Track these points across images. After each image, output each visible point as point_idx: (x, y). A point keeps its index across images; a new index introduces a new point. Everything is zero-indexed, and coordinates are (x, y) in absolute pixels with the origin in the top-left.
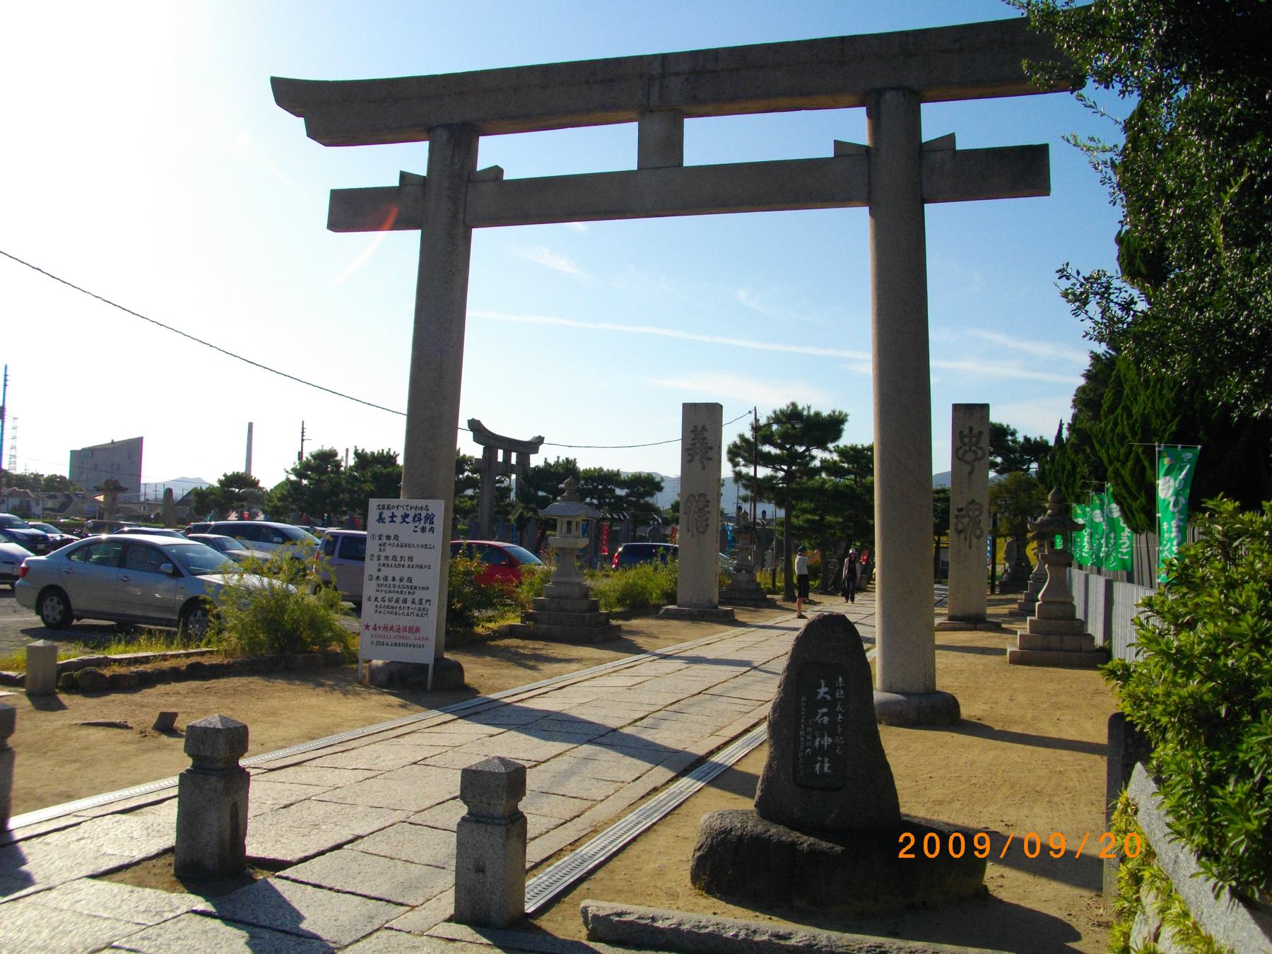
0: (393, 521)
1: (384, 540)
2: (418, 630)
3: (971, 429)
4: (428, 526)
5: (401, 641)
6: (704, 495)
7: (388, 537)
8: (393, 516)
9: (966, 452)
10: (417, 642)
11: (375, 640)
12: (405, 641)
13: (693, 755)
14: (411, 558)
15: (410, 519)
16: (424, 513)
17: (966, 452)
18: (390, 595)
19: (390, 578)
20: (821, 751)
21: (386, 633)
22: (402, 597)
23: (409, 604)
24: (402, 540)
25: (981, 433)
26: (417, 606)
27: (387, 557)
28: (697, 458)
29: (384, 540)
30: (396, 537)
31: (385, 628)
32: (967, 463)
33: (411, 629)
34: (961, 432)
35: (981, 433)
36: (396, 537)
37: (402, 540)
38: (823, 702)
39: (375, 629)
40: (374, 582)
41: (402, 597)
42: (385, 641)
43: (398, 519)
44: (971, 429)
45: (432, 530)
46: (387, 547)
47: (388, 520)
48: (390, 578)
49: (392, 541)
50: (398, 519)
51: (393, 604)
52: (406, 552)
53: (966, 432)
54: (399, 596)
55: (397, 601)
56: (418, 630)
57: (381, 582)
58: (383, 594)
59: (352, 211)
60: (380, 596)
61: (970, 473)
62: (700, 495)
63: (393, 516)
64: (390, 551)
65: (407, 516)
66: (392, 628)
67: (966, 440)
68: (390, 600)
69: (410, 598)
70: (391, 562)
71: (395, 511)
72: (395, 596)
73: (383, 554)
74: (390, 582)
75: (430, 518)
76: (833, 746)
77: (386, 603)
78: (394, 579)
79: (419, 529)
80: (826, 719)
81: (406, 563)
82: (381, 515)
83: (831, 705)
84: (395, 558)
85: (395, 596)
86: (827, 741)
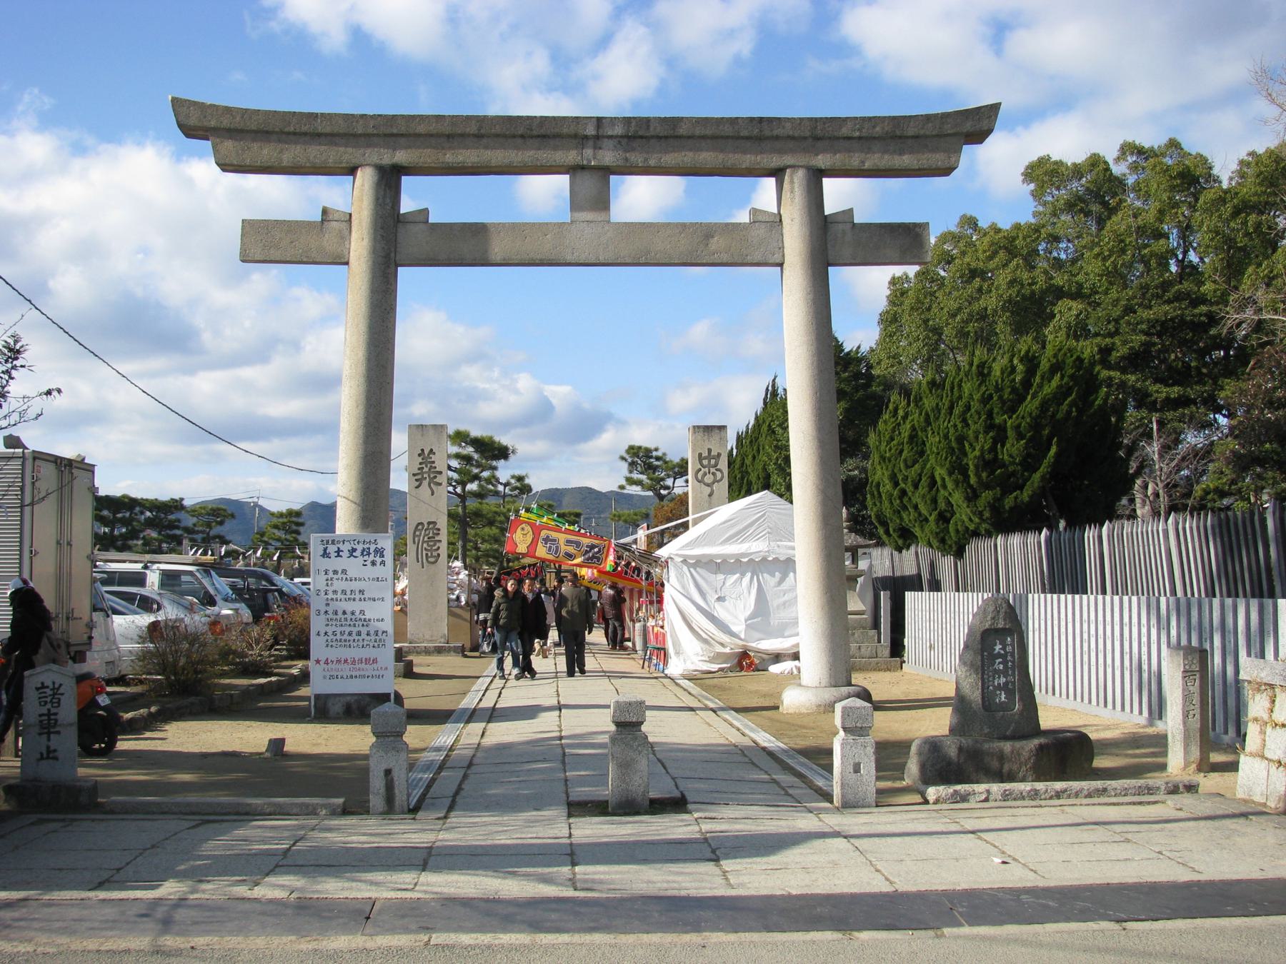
0: (339, 556)
1: (331, 575)
2: (375, 661)
3: (710, 451)
4: (378, 560)
5: (358, 673)
6: (434, 523)
7: (335, 572)
8: (339, 551)
9: (705, 474)
10: (375, 673)
11: (328, 674)
12: (362, 673)
13: (427, 809)
14: (361, 592)
15: (357, 553)
16: (373, 547)
17: (705, 474)
18: (343, 629)
19: (340, 613)
20: (999, 687)
21: (340, 666)
22: (355, 630)
23: (364, 636)
24: (351, 574)
25: (719, 455)
26: (373, 638)
27: (335, 592)
28: (425, 483)
29: (331, 575)
30: (344, 572)
31: (339, 661)
32: (708, 485)
33: (367, 661)
34: (700, 455)
35: (719, 455)
36: (344, 572)
37: (351, 574)
38: (999, 655)
39: (327, 662)
40: (323, 616)
41: (355, 630)
42: (340, 674)
43: (345, 554)
44: (710, 451)
45: (383, 563)
46: (335, 582)
47: (333, 555)
48: (340, 613)
49: (340, 576)
50: (345, 554)
51: (345, 637)
52: (356, 586)
53: (705, 454)
54: (352, 629)
55: (350, 634)
56: (375, 661)
57: (331, 616)
58: (334, 628)
59: (267, 243)
60: (330, 630)
61: (710, 495)
62: (429, 523)
63: (339, 551)
64: (339, 585)
65: (354, 550)
66: (346, 661)
67: (705, 462)
68: (342, 633)
69: (364, 630)
70: (339, 596)
71: (341, 546)
72: (347, 629)
73: (331, 589)
74: (340, 615)
75: (380, 552)
76: (1006, 684)
77: (338, 637)
78: (353, 613)
79: (368, 563)
80: (1001, 667)
81: (358, 596)
82: (325, 550)
83: (1004, 657)
84: (344, 592)
85: (347, 629)
86: (1003, 680)
